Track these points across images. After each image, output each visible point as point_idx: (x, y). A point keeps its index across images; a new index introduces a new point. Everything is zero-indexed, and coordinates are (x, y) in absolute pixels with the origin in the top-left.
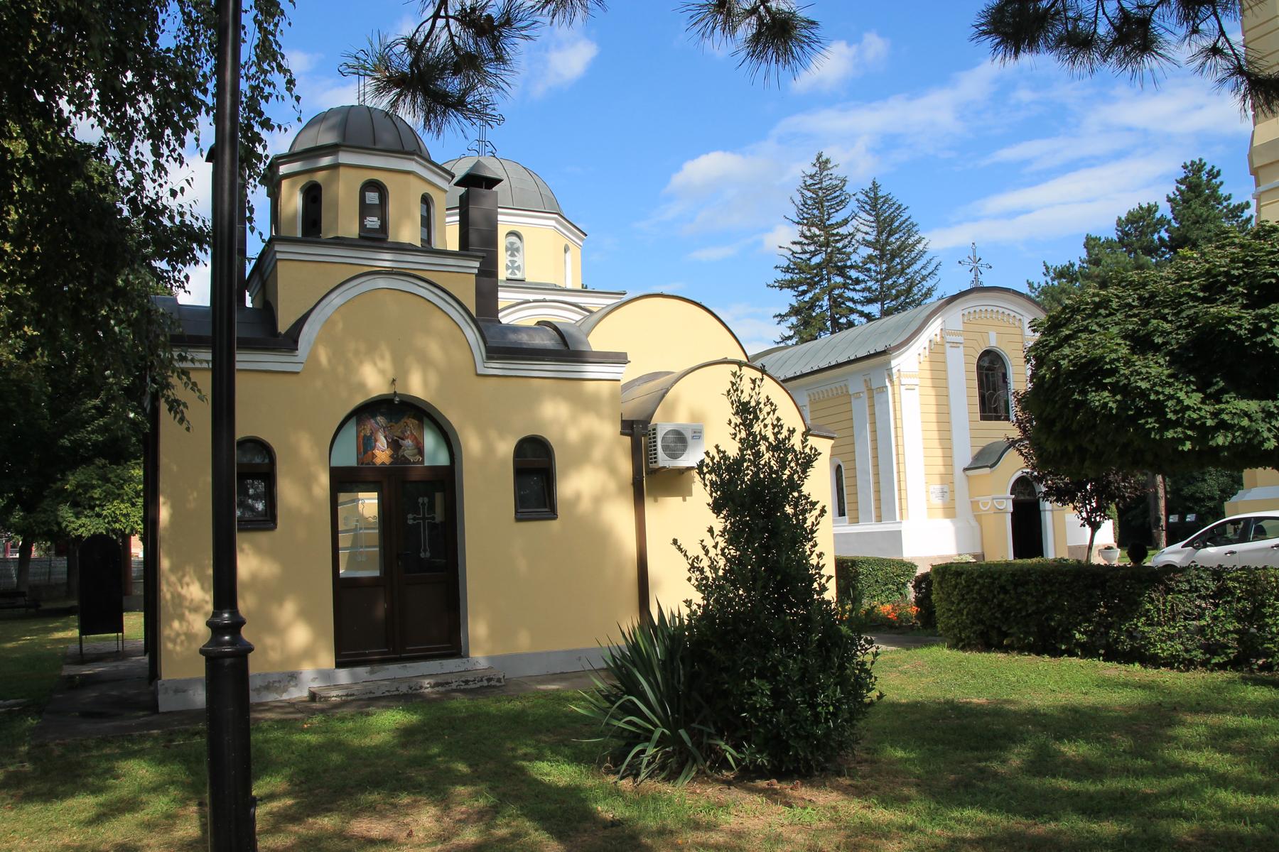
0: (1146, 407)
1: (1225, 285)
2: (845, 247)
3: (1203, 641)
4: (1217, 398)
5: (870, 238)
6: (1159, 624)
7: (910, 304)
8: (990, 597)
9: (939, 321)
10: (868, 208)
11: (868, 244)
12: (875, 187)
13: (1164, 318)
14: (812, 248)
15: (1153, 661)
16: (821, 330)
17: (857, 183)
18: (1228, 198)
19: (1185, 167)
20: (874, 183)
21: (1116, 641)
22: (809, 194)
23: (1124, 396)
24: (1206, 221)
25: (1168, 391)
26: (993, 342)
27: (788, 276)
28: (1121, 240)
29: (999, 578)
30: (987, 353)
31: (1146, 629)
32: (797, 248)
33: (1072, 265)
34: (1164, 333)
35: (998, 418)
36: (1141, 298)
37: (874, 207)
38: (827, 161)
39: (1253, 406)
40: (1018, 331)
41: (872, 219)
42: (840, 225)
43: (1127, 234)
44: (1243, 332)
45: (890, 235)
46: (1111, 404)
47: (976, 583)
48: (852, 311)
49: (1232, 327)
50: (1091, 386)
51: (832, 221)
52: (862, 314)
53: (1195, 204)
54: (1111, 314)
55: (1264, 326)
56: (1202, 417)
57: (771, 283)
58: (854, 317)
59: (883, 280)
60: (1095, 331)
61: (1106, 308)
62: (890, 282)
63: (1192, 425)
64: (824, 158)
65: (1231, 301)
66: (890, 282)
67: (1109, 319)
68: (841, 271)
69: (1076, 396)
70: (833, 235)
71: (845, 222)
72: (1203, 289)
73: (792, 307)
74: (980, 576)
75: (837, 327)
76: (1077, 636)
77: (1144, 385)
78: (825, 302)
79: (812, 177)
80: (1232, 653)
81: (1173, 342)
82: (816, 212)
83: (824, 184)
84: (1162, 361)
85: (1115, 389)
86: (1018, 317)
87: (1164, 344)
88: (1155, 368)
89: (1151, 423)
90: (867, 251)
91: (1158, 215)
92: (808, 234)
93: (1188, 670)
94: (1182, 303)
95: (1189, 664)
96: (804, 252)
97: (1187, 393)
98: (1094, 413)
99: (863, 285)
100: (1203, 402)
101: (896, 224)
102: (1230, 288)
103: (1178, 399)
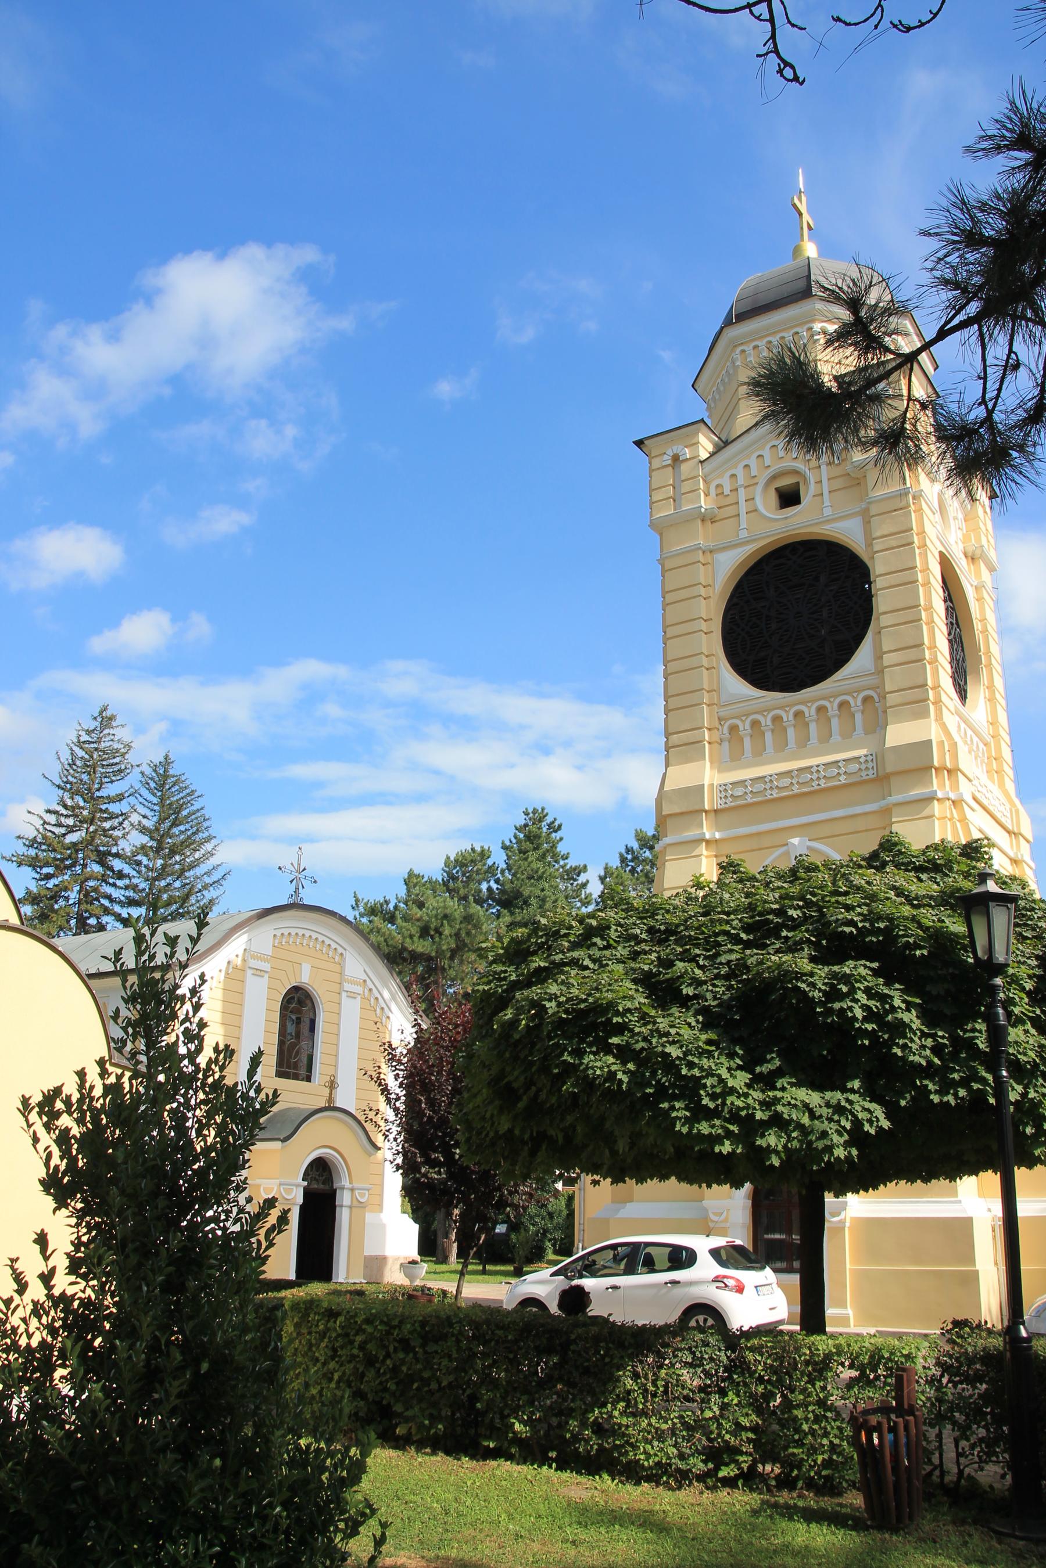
0: (673, 1085)
1: (779, 927)
2: (113, 828)
3: (705, 1442)
4: (767, 1082)
5: (149, 824)
6: (644, 1413)
7: (182, 915)
8: (381, 1355)
9: (244, 938)
10: (152, 785)
11: (143, 830)
12: (167, 762)
13: (693, 959)
14: (70, 822)
15: (633, 1473)
16: (61, 928)
17: (144, 751)
18: (565, 857)
19: (526, 814)
20: (166, 757)
21: (576, 1438)
22: (80, 753)
23: (639, 1066)
24: (540, 878)
25: (705, 1062)
26: (305, 977)
27: (32, 852)
28: (445, 884)
29: (356, 1315)
30: (296, 989)
31: (624, 1421)
32: (52, 819)
33: (387, 902)
34: (698, 983)
35: (296, 1077)
36: (651, 930)
37: (161, 786)
38: (111, 718)
39: (814, 1098)
40: (337, 968)
41: (155, 800)
42: (110, 800)
43: (453, 878)
44: (817, 994)
45: (174, 824)
46: (620, 1075)
47: (360, 1331)
48: (107, 911)
49: (803, 986)
50: (590, 1045)
51: (103, 793)
52: (118, 917)
53: (532, 856)
54: (608, 947)
55: (845, 989)
56: (748, 1107)
57: (8, 855)
58: (105, 919)
59: (155, 879)
60: (587, 968)
61: (603, 939)
62: (163, 883)
63: (734, 1117)
64: (108, 713)
65: (794, 948)
66: (163, 883)
67: (607, 953)
68: (102, 858)
69: (566, 1057)
70: (101, 810)
71: (120, 798)
72: (747, 928)
73: (29, 892)
74: (368, 1321)
75: (83, 927)
76: (518, 1427)
77: (674, 1052)
78: (73, 895)
79: (89, 732)
80: (745, 1461)
81: (709, 996)
82: (85, 777)
83: (103, 745)
84: (692, 1020)
85: (624, 1054)
86: (340, 950)
87: (696, 997)
88: (681, 1032)
89: (680, 1110)
90: (138, 839)
91: (490, 862)
92: (69, 802)
93: (679, 1488)
94: (719, 945)
95: (683, 1478)
96: (59, 825)
97: (729, 1069)
98: (589, 1084)
99: (127, 881)
100: (749, 1086)
101: (184, 813)
102: (784, 933)
103: (719, 1076)
